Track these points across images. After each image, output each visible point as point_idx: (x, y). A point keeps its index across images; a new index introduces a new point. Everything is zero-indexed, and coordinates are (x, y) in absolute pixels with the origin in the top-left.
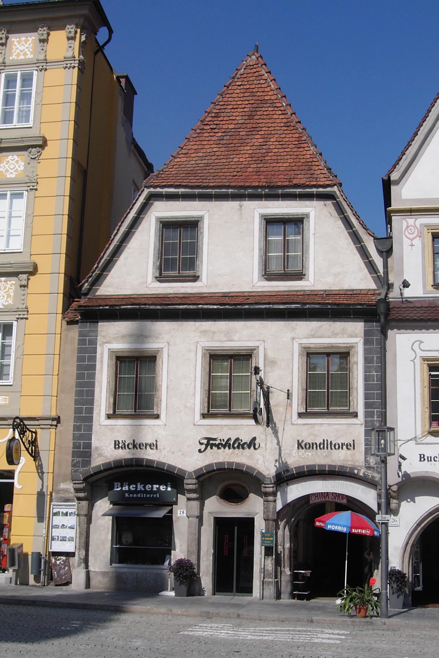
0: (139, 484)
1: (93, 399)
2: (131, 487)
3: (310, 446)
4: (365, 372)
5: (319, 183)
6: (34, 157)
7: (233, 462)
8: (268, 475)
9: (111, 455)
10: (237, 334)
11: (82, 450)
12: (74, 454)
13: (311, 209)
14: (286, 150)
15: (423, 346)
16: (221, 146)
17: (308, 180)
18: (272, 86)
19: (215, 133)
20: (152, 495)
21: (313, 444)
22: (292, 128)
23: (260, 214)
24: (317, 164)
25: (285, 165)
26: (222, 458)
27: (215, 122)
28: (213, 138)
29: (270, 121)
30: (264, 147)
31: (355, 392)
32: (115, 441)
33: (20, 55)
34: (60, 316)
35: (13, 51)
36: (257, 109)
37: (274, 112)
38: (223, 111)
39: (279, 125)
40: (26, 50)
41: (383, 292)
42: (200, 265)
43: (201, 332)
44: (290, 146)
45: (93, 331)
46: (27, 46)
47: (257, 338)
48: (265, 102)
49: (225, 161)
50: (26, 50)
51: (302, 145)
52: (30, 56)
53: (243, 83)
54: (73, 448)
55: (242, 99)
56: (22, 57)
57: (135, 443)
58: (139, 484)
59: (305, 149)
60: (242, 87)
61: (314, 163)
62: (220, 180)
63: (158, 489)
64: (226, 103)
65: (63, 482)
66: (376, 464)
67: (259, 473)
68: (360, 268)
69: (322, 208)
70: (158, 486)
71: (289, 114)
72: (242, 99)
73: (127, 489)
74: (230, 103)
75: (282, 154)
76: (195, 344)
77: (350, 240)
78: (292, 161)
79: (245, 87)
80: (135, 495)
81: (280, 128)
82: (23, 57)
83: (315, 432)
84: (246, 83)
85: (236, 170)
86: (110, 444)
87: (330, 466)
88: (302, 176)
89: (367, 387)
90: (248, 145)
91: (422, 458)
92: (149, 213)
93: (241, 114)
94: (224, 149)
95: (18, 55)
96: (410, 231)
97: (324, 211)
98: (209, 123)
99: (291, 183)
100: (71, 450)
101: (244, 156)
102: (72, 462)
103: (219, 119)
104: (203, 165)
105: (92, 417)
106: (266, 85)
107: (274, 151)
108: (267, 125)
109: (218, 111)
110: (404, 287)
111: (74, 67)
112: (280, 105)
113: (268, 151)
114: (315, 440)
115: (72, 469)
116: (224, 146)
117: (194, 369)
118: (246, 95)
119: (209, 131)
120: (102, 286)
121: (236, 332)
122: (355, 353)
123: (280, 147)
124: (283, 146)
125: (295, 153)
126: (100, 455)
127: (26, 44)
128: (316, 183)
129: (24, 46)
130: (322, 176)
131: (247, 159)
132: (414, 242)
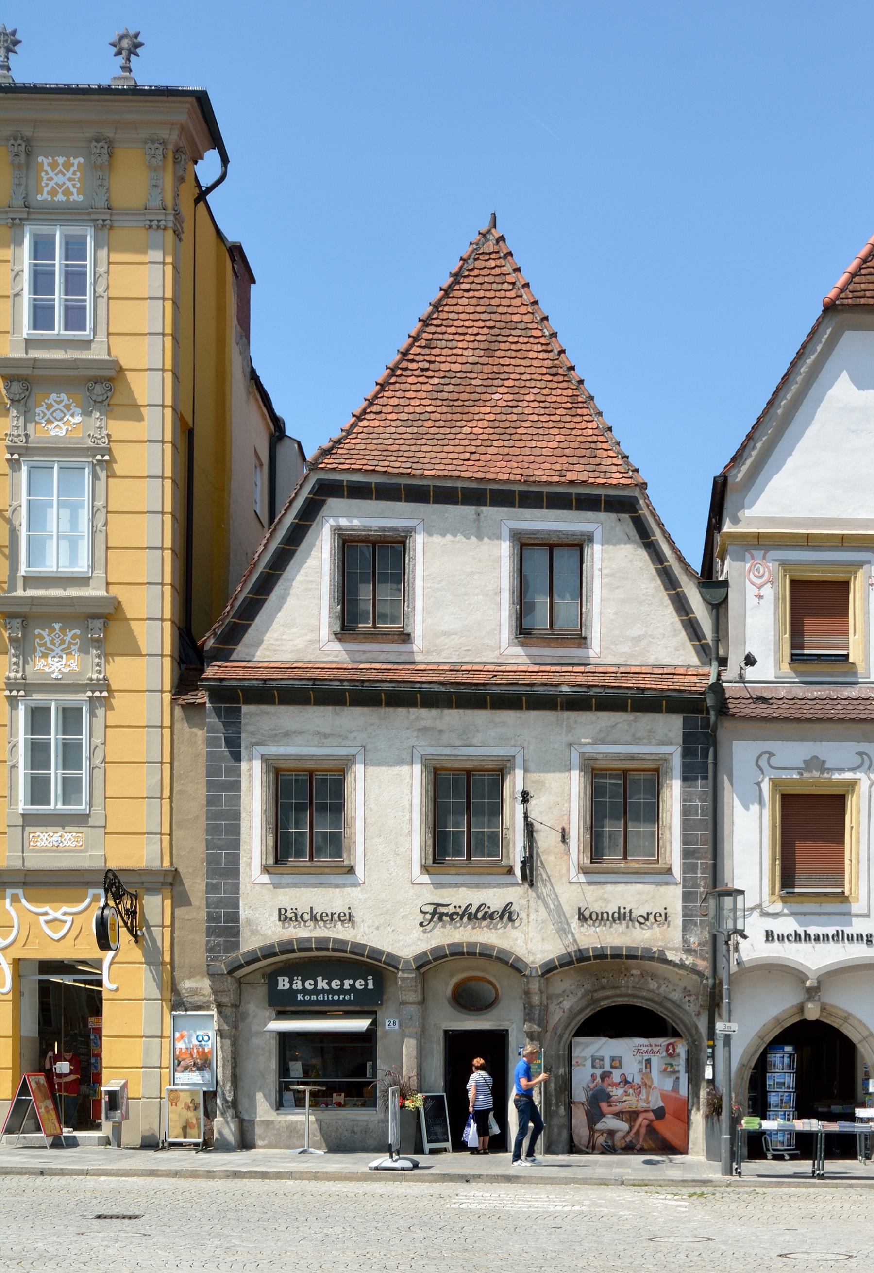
0: (319, 979)
1: (239, 840)
2: (287, 986)
3: (298, 918)
4: (684, 801)
5: (610, 481)
6: (100, 399)
7: (476, 943)
8: (533, 962)
9: (274, 933)
10: (480, 736)
11: (225, 925)
12: (210, 932)
13: (597, 525)
14: (552, 418)
15: (774, 761)
16: (439, 403)
17: (591, 474)
18: (525, 296)
19: (427, 377)
20: (341, 997)
21: (602, 913)
22: (561, 378)
23: (511, 530)
24: (605, 446)
25: (550, 445)
26: (457, 937)
27: (427, 358)
28: (425, 388)
29: (523, 362)
30: (515, 410)
31: (667, 832)
32: (280, 910)
33: (58, 192)
34: (167, 697)
35: (43, 185)
36: (500, 338)
37: (528, 347)
38: (441, 336)
39: (539, 371)
41: (713, 670)
42: (411, 614)
43: (419, 730)
44: (559, 412)
45: (233, 722)
47: (512, 743)
48: (513, 325)
49: (448, 431)
50: (69, 184)
51: (579, 411)
52: (76, 197)
53: (473, 286)
54: (208, 921)
55: (472, 317)
56: (60, 197)
57: (315, 912)
58: (319, 979)
59: (585, 418)
60: (471, 294)
61: (599, 445)
62: (442, 467)
63: (353, 986)
64: (444, 323)
65: (189, 978)
66: (699, 944)
67: (518, 959)
68: (675, 631)
69: (613, 524)
70: (351, 982)
71: (556, 351)
72: (472, 317)
73: (300, 987)
74: (451, 323)
75: (546, 425)
76: (410, 751)
77: (659, 582)
78: (563, 438)
79: (477, 294)
80: (314, 997)
81: (540, 377)
82: (64, 199)
83: (606, 896)
84: (479, 287)
85: (469, 449)
86: (271, 915)
87: (628, 948)
88: (581, 468)
89: (686, 825)
90: (487, 403)
91: (769, 936)
92: (318, 517)
93: (471, 345)
94: (444, 409)
96: (756, 573)
97: (617, 529)
98: (417, 358)
99: (563, 480)
100: (204, 925)
101: (480, 424)
102: (207, 945)
103: (434, 352)
104: (410, 436)
106: (512, 294)
107: (531, 418)
108: (518, 370)
109: (430, 336)
110: (746, 664)
111: (165, 229)
112: (539, 334)
113: (521, 417)
114: (606, 907)
115: (208, 957)
116: (444, 403)
117: (409, 791)
118: (479, 309)
119: (416, 373)
120: (240, 644)
121: (478, 731)
122: (669, 770)
123: (542, 411)
124: (547, 411)
125: (567, 425)
126: (254, 932)
127: (68, 171)
128: (604, 481)
129: (64, 175)
130: (614, 469)
131: (486, 431)
132: (763, 592)
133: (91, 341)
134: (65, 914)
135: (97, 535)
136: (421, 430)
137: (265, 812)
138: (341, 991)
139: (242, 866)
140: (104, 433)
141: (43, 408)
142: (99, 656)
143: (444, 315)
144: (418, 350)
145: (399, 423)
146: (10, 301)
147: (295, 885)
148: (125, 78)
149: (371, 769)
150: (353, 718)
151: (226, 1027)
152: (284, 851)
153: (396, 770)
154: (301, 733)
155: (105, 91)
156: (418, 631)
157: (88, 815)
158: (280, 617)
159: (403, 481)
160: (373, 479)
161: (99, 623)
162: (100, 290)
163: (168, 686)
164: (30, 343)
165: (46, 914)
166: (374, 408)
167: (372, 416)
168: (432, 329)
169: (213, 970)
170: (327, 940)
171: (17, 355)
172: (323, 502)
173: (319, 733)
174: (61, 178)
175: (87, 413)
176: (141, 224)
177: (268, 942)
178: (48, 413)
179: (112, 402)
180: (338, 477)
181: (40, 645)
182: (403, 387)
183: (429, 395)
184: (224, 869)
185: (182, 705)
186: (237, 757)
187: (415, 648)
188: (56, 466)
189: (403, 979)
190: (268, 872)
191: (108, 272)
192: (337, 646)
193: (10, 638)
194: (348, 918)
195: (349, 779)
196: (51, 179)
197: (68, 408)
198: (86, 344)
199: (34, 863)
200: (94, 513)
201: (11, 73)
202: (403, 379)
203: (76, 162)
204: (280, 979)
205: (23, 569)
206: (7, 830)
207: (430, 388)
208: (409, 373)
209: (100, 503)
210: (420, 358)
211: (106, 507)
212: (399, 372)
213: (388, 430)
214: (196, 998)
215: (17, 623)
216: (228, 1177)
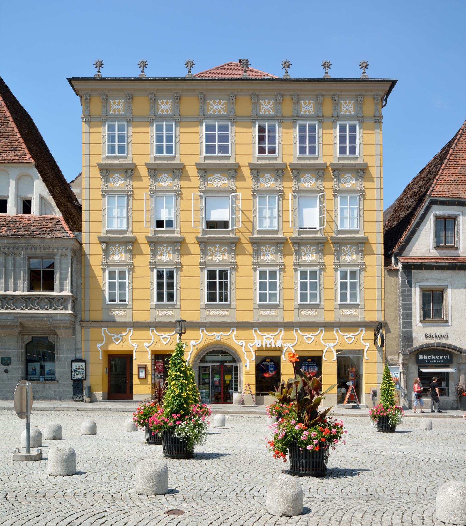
0: (432, 356)
2: (422, 358)
3: (431, 337)
6: (233, 175)
11: (408, 339)
12: (403, 341)
28: (456, 170)
34: (383, 267)
40: (270, 109)
46: (350, 106)
50: (350, 109)
56: (347, 113)
58: (432, 356)
63: (443, 358)
80: (431, 361)
95: (345, 112)
98: (453, 161)
105: (412, 322)
126: (417, 341)
133: (175, 157)
134: (168, 336)
135: (361, 218)
136: (458, 183)
137: (420, 303)
138: (439, 359)
139: (413, 321)
140: (363, 186)
141: (344, 179)
142: (362, 255)
143: (458, 147)
144: (452, 158)
145: (450, 181)
146: (333, 145)
147: (430, 326)
148: (99, 75)
149: (453, 290)
150: (447, 274)
151: (405, 371)
152: (425, 315)
153: (461, 290)
154: (431, 279)
155: (92, 79)
156: (460, 247)
157: (359, 305)
158: (417, 243)
159: (457, 200)
160: (448, 199)
161: (361, 245)
162: (233, 141)
163: (383, 264)
164: (156, 158)
165: (346, 335)
166: (442, 177)
167: (441, 179)
168: (455, 151)
169: (404, 353)
170: (440, 343)
171: (201, 162)
172: (431, 207)
173: (437, 279)
174: (308, 107)
175: (357, 180)
176: (197, 120)
177: (421, 344)
178: (345, 180)
179: (365, 176)
180: (437, 199)
181: (344, 252)
182: (449, 170)
183: (458, 172)
184: (408, 322)
185: (387, 270)
186: (411, 287)
187: (460, 252)
188: (349, 197)
189: (463, 356)
190: (421, 322)
191: (235, 136)
192: (435, 251)
193: (335, 250)
194: (446, 337)
195: (446, 293)
196: (344, 108)
197: (351, 178)
198: (173, 158)
199: (342, 320)
200: (279, 211)
201: (288, 74)
202: (449, 167)
203: (352, 102)
204: (420, 356)
205: (257, 228)
206: (150, 309)
207: (458, 170)
208: (450, 165)
209: (178, 207)
210: (453, 161)
211: (132, 208)
212: (447, 165)
213: (447, 183)
214: (393, 362)
215: (105, 245)
216: (450, 417)
